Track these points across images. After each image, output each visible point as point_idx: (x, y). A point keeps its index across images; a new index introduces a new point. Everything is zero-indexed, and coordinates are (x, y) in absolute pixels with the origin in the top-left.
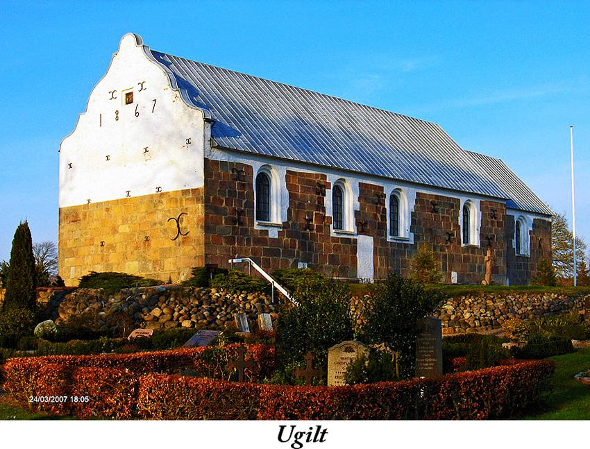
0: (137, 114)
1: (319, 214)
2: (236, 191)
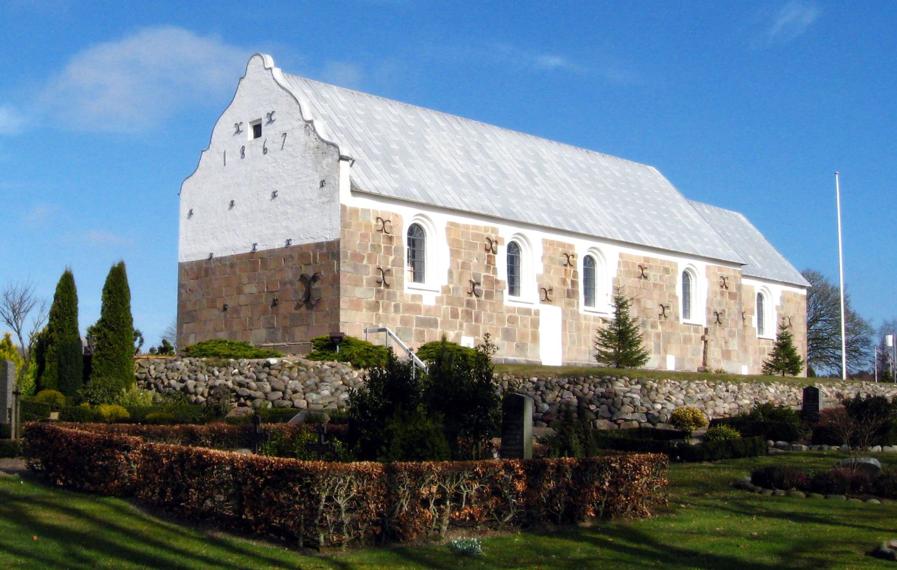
0: (265, 151)
1: (488, 276)
2: (380, 246)
